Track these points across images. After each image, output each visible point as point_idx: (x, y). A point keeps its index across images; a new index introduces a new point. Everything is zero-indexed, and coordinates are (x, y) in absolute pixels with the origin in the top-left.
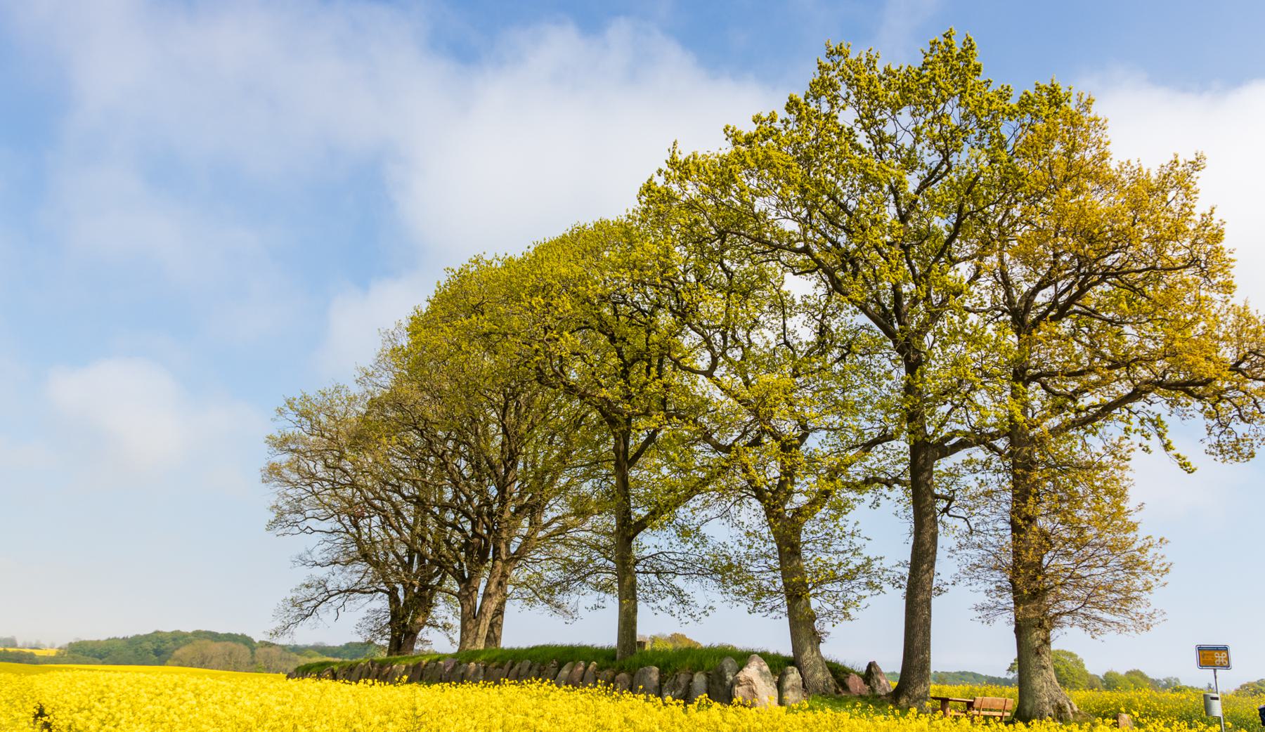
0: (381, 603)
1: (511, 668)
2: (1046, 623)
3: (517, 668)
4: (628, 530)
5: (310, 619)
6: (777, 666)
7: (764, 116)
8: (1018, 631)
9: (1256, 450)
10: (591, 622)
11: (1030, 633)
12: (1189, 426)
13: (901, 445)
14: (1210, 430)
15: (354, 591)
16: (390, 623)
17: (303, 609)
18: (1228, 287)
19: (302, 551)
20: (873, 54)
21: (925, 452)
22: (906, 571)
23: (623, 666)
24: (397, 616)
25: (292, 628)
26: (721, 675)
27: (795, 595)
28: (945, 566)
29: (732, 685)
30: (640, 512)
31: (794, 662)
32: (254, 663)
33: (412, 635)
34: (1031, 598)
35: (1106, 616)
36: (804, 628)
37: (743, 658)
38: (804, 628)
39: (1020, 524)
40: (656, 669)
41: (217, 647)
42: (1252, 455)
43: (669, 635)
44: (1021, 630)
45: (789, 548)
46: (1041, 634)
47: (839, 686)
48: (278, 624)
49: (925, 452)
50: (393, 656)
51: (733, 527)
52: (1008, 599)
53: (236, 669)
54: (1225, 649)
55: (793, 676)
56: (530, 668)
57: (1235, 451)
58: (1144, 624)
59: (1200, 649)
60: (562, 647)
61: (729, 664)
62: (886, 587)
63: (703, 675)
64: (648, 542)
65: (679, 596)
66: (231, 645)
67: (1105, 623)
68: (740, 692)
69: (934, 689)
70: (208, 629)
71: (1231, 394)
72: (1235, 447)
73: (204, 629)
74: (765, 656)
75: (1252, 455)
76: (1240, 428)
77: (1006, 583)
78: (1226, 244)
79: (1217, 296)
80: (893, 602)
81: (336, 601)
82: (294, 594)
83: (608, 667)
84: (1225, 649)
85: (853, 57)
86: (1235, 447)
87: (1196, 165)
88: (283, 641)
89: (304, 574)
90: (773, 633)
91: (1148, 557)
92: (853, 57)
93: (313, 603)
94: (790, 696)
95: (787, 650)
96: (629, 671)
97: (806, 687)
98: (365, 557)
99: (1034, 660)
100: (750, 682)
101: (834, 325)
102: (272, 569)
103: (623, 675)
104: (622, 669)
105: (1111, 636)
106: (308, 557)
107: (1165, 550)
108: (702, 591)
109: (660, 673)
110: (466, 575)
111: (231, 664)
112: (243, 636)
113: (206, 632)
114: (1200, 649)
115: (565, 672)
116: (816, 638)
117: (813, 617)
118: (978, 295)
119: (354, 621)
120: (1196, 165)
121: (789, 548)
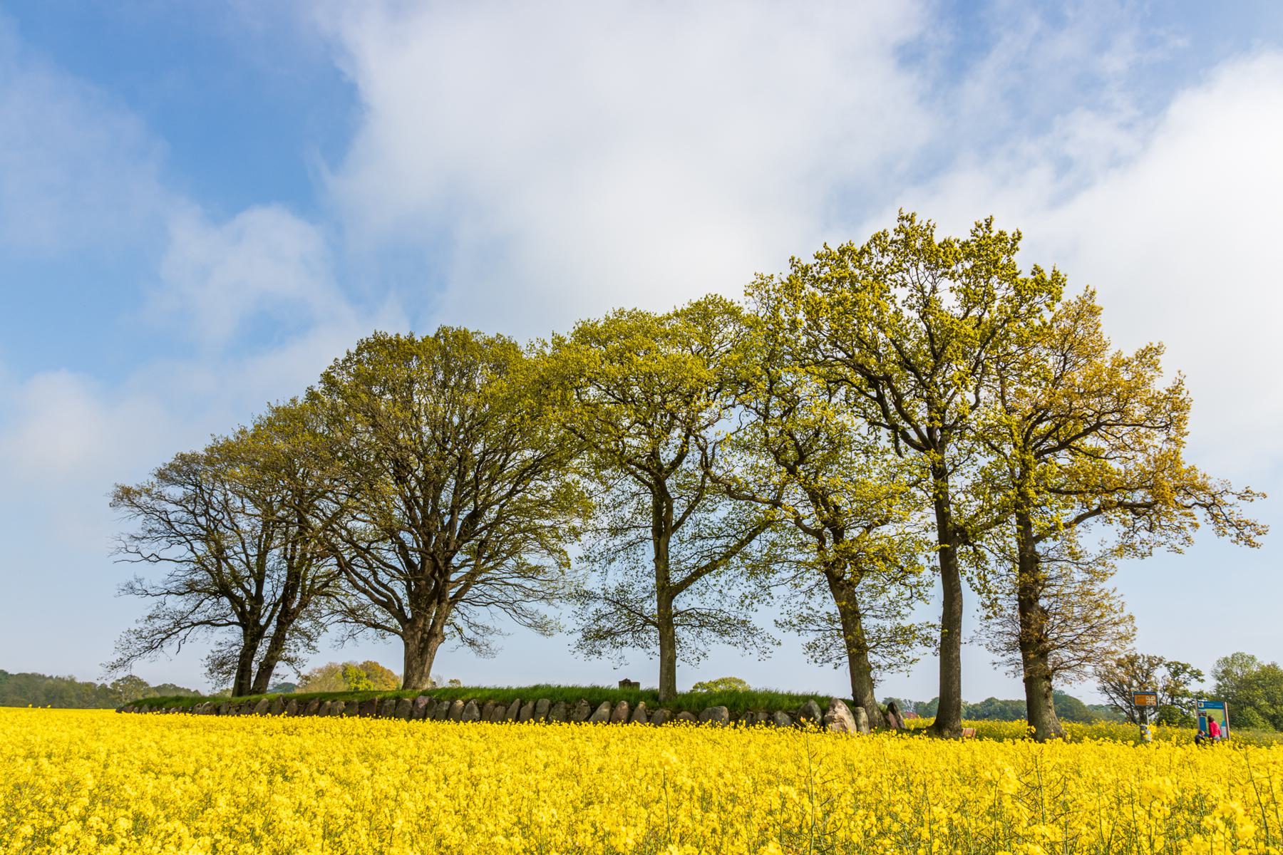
0: (232, 636)
1: (521, 707)
5: (153, 653)
10: (638, 664)
11: (1036, 681)
16: (279, 659)
17: (153, 642)
20: (931, 224)
23: (663, 706)
27: (857, 652)
30: (676, 578)
33: (267, 669)
34: (1033, 648)
36: (861, 675)
38: (861, 675)
43: (360, 662)
44: (1029, 682)
45: (850, 617)
47: (888, 718)
48: (114, 659)
50: (248, 691)
60: (580, 689)
63: (802, 712)
64: (682, 602)
69: (967, 725)
70: (542, 682)
74: (843, 700)
80: (927, 663)
82: (142, 625)
87: (1157, 351)
89: (148, 605)
97: (871, 724)
100: (841, 720)
102: (103, 596)
103: (685, 713)
106: (137, 586)
109: (730, 711)
110: (410, 616)
116: (871, 684)
119: (193, 662)
121: (850, 617)
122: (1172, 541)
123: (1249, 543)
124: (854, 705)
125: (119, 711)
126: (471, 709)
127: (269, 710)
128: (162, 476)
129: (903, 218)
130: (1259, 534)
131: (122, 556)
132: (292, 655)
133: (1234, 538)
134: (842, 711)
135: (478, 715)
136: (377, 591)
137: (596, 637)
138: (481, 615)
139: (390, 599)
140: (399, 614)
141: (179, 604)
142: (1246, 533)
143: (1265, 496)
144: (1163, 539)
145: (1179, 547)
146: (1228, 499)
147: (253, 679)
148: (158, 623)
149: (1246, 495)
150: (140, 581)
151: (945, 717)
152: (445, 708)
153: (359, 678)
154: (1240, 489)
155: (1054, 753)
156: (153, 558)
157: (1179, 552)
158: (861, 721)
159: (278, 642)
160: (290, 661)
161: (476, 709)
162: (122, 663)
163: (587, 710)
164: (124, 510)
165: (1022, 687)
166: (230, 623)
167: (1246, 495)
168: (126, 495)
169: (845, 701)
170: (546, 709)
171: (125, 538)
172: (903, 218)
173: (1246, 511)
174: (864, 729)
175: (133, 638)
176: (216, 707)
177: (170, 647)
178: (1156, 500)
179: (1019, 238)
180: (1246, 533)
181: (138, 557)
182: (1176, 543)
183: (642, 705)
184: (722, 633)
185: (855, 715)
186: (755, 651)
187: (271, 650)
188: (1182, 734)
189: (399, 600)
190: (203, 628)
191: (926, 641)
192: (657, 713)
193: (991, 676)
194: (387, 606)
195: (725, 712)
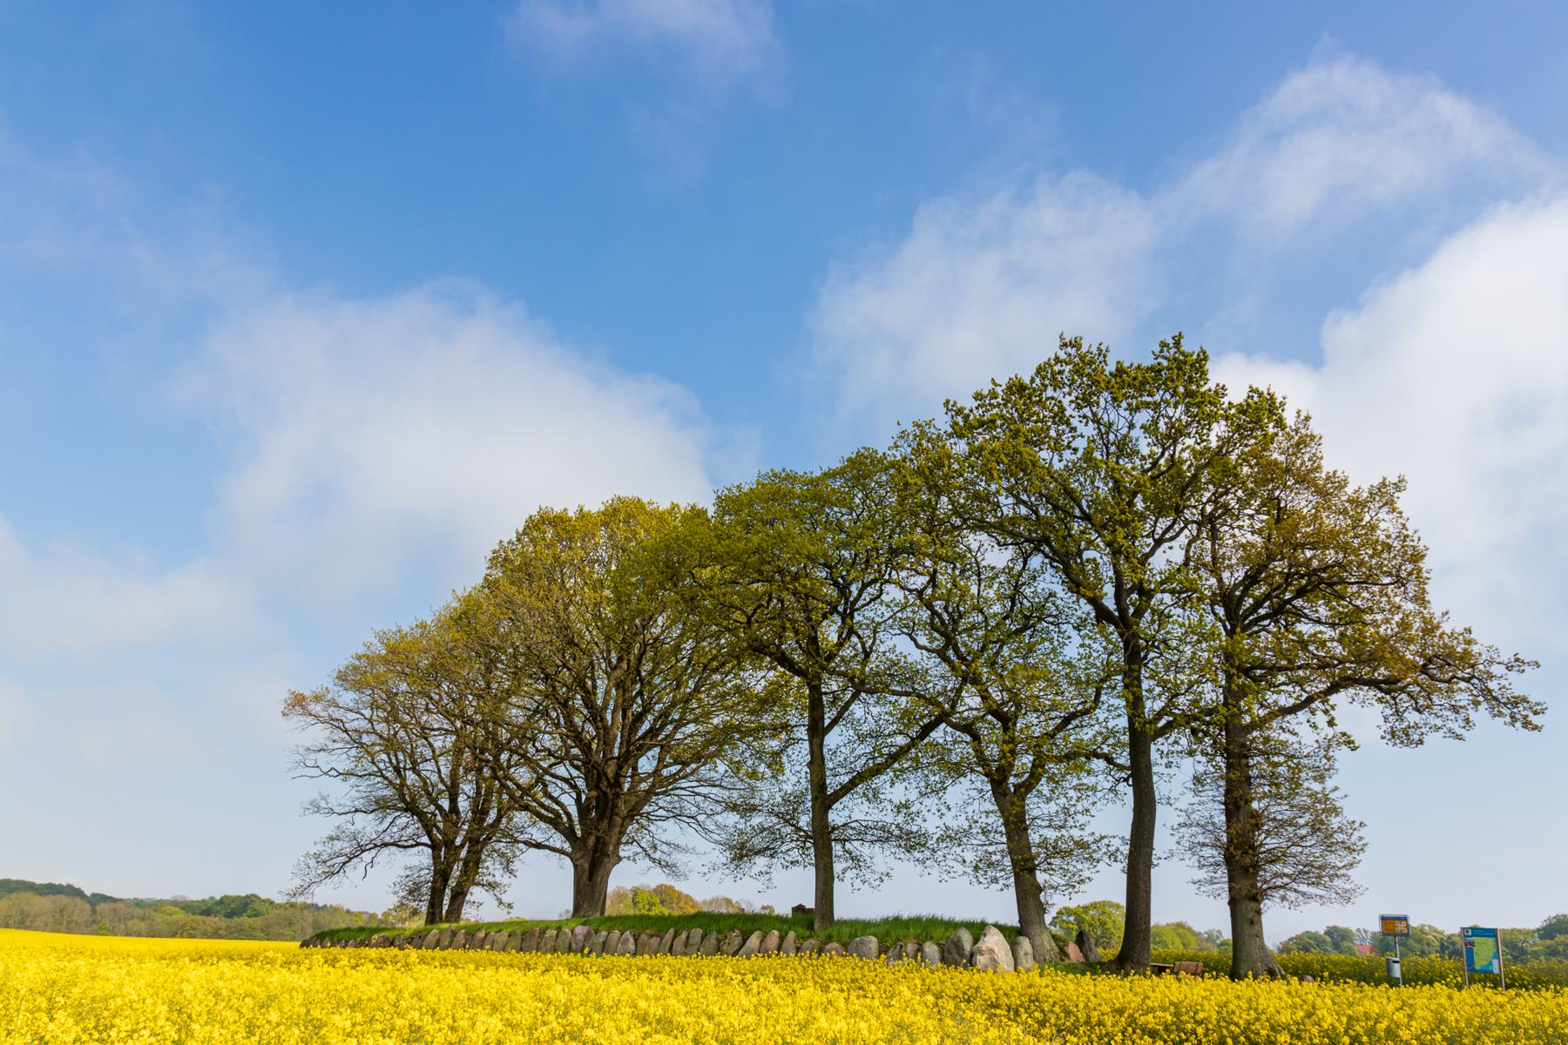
0: (421, 858)
2: (1256, 897)
3: (684, 935)
4: (824, 800)
5: (336, 878)
6: (1012, 935)
7: (985, 392)
8: (1233, 903)
9: (1425, 739)
10: (785, 886)
11: (1245, 904)
12: (1358, 712)
13: (1112, 716)
14: (1386, 719)
15: (386, 845)
17: (333, 867)
18: (1420, 599)
19: (316, 796)
20: (1103, 347)
21: (1140, 738)
22: (1126, 849)
23: (815, 927)
24: (442, 874)
25: (314, 887)
26: (958, 945)
28: (1163, 840)
29: (972, 955)
30: (833, 784)
31: (1020, 932)
32: (94, 922)
33: (459, 895)
34: (1244, 868)
35: (1312, 890)
36: (1029, 896)
37: (978, 929)
38: (1029, 896)
39: (1235, 804)
40: (874, 939)
41: (45, 903)
42: (1421, 742)
43: (653, 886)
45: (1016, 826)
46: (1253, 905)
48: (297, 882)
49: (1140, 738)
51: (968, 799)
52: (1222, 873)
53: (69, 931)
54: (1405, 919)
55: (1025, 944)
56: (703, 937)
57: (1401, 736)
58: (1346, 897)
59: (1384, 919)
61: (966, 938)
62: (1106, 859)
63: (950, 943)
64: (836, 817)
65: (855, 860)
66: (63, 899)
67: (1304, 894)
68: (981, 960)
71: (1411, 688)
72: (1406, 732)
73: (27, 879)
74: (996, 925)
75: (1421, 742)
76: (1412, 717)
77: (1221, 858)
78: (1425, 565)
79: (1409, 606)
81: (367, 856)
82: (320, 847)
83: (811, 937)
84: (1405, 919)
85: (1084, 349)
86: (1406, 732)
87: (1398, 486)
88: (300, 900)
89: (329, 825)
90: (1000, 905)
91: (1354, 838)
92: (1084, 349)
93: (343, 859)
94: (1027, 962)
95: (1013, 919)
96: (839, 941)
98: (411, 808)
99: (1247, 930)
100: (991, 951)
101: (1028, 591)
102: (282, 808)
103: (835, 945)
104: (829, 939)
105: (1314, 905)
106: (323, 804)
107: (1362, 832)
108: (880, 857)
110: (579, 833)
111: (62, 923)
112: (69, 886)
113: (17, 882)
114: (1384, 919)
115: (754, 940)
117: (1040, 889)
118: (1177, 584)
119: (381, 883)
120: (1398, 486)
121: (1016, 826)
122: (1450, 725)
123: (1526, 724)
124: (1012, 935)
125: (305, 944)
126: (627, 940)
127: (570, 950)
128: (342, 677)
129: (1065, 345)
130: (1536, 713)
131: (301, 771)
132: (490, 879)
133: (1508, 719)
134: (994, 941)
135: (633, 947)
136: (542, 806)
137: (742, 853)
138: (668, 831)
139: (558, 815)
140: (569, 833)
141: (368, 825)
142: (1519, 712)
143: (1537, 664)
144: (1439, 722)
145: (1459, 731)
146: (1497, 670)
147: (445, 908)
148: (338, 845)
149: (1517, 664)
150: (324, 798)
151: (1133, 946)
152: (602, 940)
153: (651, 904)
154: (1506, 656)
155: (1244, 988)
156: (333, 773)
157: (1459, 737)
158: (1021, 954)
159: (473, 864)
160: (492, 886)
161: (631, 940)
162: (303, 890)
163: (738, 941)
164: (297, 720)
165: (1227, 910)
166: (418, 844)
167: (1517, 664)
168: (298, 702)
169: (1002, 929)
170: (698, 939)
171: (301, 751)
172: (1065, 345)
173: (1518, 684)
174: (1027, 962)
175: (312, 863)
176: (416, 940)
177: (355, 870)
178: (1425, 673)
179: (1206, 359)
180: (1519, 712)
181: (317, 772)
182: (1455, 727)
183: (792, 935)
184: (909, 849)
185: (1014, 947)
186: (935, 871)
187: (465, 872)
188: (441, 932)
189: (568, 815)
190: (393, 849)
191: (1113, 856)
192: (806, 944)
193: (1189, 901)
194: (555, 822)
195: (931, 949)
